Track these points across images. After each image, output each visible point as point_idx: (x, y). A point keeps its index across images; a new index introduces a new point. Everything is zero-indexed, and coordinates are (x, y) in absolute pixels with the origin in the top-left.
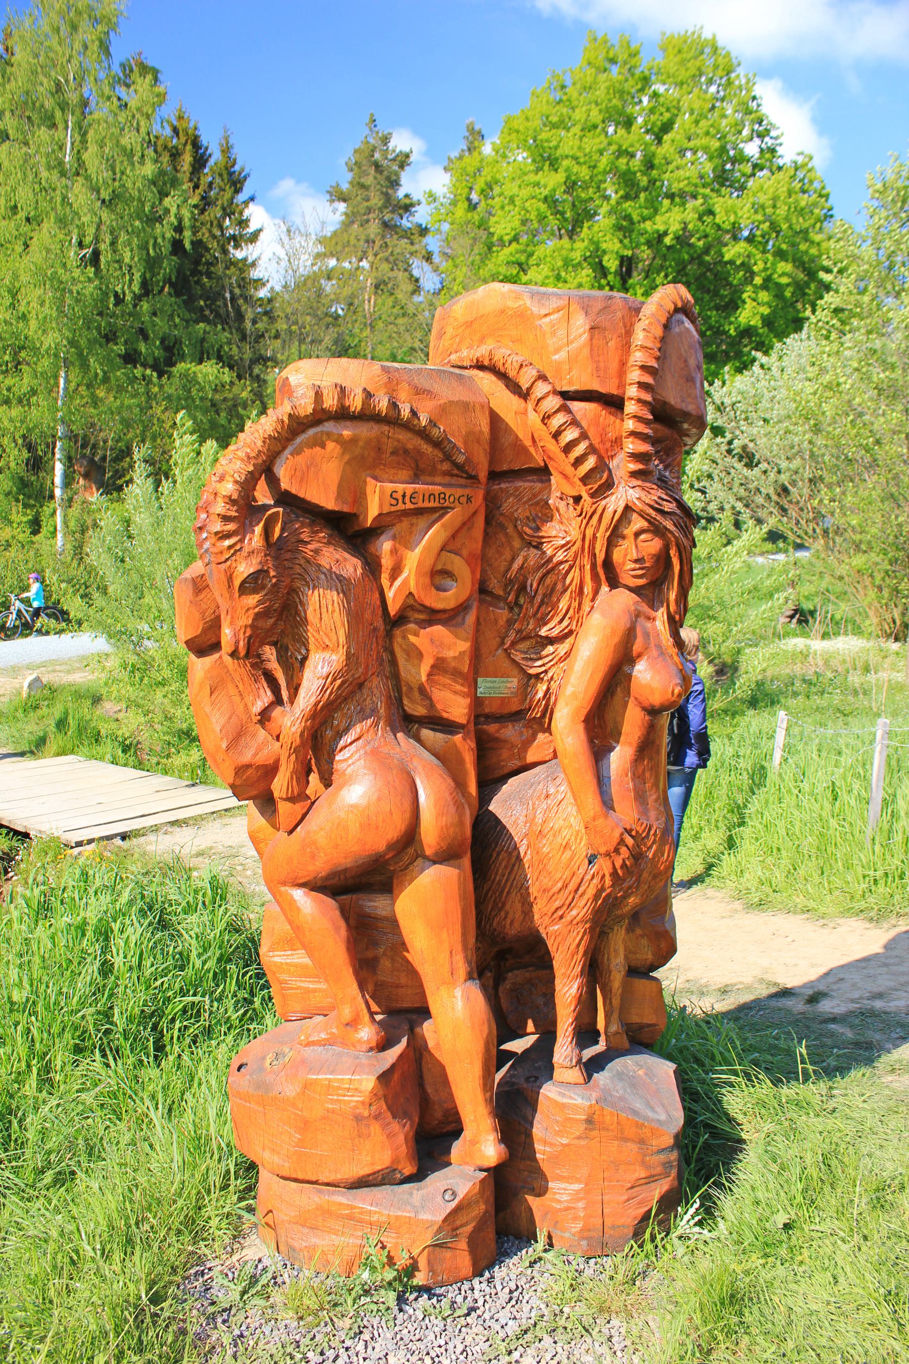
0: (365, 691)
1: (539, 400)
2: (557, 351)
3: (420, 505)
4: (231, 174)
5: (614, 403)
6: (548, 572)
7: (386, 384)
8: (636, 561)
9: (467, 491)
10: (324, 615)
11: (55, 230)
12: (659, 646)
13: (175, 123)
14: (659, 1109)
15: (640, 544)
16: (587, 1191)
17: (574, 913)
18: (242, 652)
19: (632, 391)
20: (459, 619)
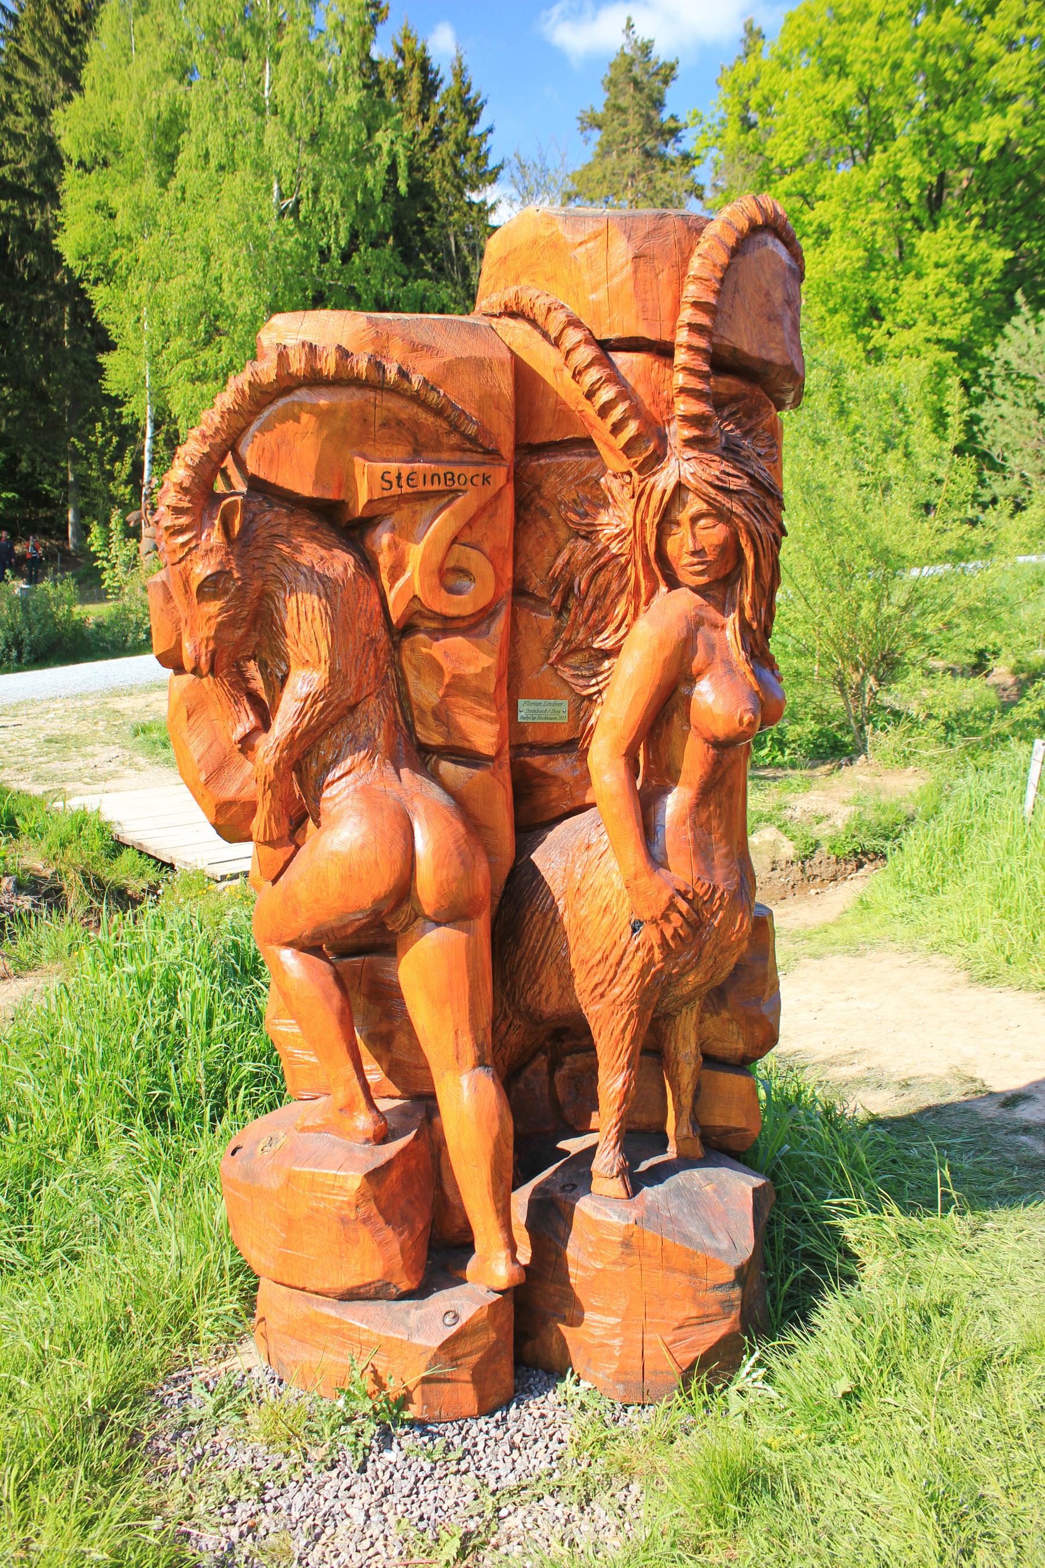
0: (358, 715)
1: (568, 353)
2: (595, 289)
3: (421, 488)
4: (465, 102)
5: (664, 351)
6: (600, 569)
7: (373, 341)
8: (694, 554)
9: (483, 470)
10: (303, 624)
11: (250, 179)
12: (727, 662)
13: (401, 44)
14: (722, 1236)
15: (699, 532)
16: (626, 1327)
17: (617, 991)
18: (204, 667)
19: (683, 336)
20: (483, 627)
